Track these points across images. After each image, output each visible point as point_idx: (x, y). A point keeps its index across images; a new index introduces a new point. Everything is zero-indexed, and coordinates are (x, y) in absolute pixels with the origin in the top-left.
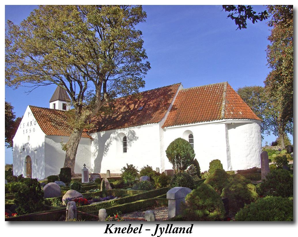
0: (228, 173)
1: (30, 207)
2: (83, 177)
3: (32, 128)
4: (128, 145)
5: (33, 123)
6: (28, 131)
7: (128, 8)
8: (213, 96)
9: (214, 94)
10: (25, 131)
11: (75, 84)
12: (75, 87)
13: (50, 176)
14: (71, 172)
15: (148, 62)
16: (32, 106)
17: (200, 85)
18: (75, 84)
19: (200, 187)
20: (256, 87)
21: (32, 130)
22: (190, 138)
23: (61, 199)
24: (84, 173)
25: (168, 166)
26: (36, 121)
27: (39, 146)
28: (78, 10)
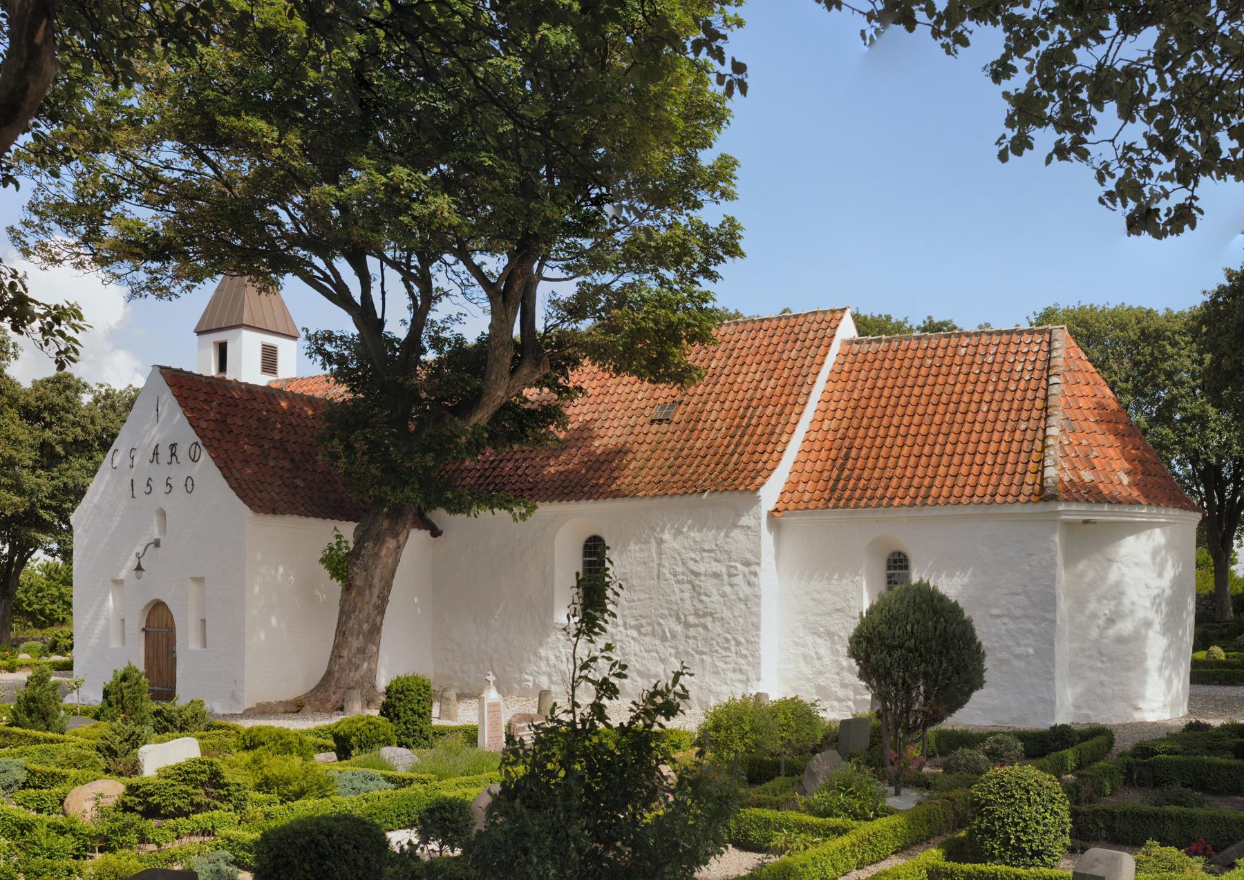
0: (391, 543)
1: (317, 455)
2: (1058, 657)
3: (179, 474)
4: (1104, 717)
5: (182, 452)
6: (159, 487)
7: (204, 425)
8: (1001, 386)
9: (1004, 376)
10: (141, 486)
11: (382, 285)
12: (383, 299)
13: (1054, 728)
14: (1172, 852)
15: (731, 221)
16: (129, 406)
17: (557, 549)
18: (382, 285)
19: (456, 220)
20: (1195, 313)
21: (178, 484)
22: (895, 568)
23: (272, 203)
24: (1055, 604)
25: (340, 392)
26: (200, 442)
27: (622, 724)
28: (459, 241)
